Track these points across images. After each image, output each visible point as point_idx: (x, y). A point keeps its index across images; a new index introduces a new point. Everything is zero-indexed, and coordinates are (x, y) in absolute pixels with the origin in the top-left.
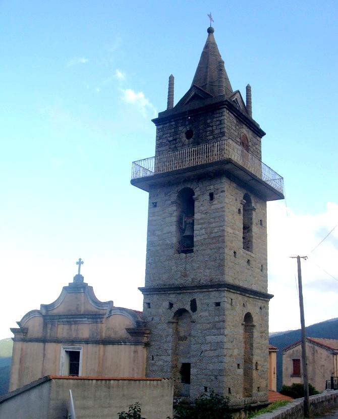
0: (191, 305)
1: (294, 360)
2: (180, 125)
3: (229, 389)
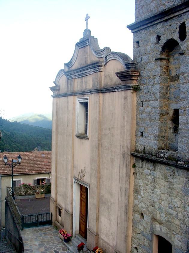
0: (180, 32)
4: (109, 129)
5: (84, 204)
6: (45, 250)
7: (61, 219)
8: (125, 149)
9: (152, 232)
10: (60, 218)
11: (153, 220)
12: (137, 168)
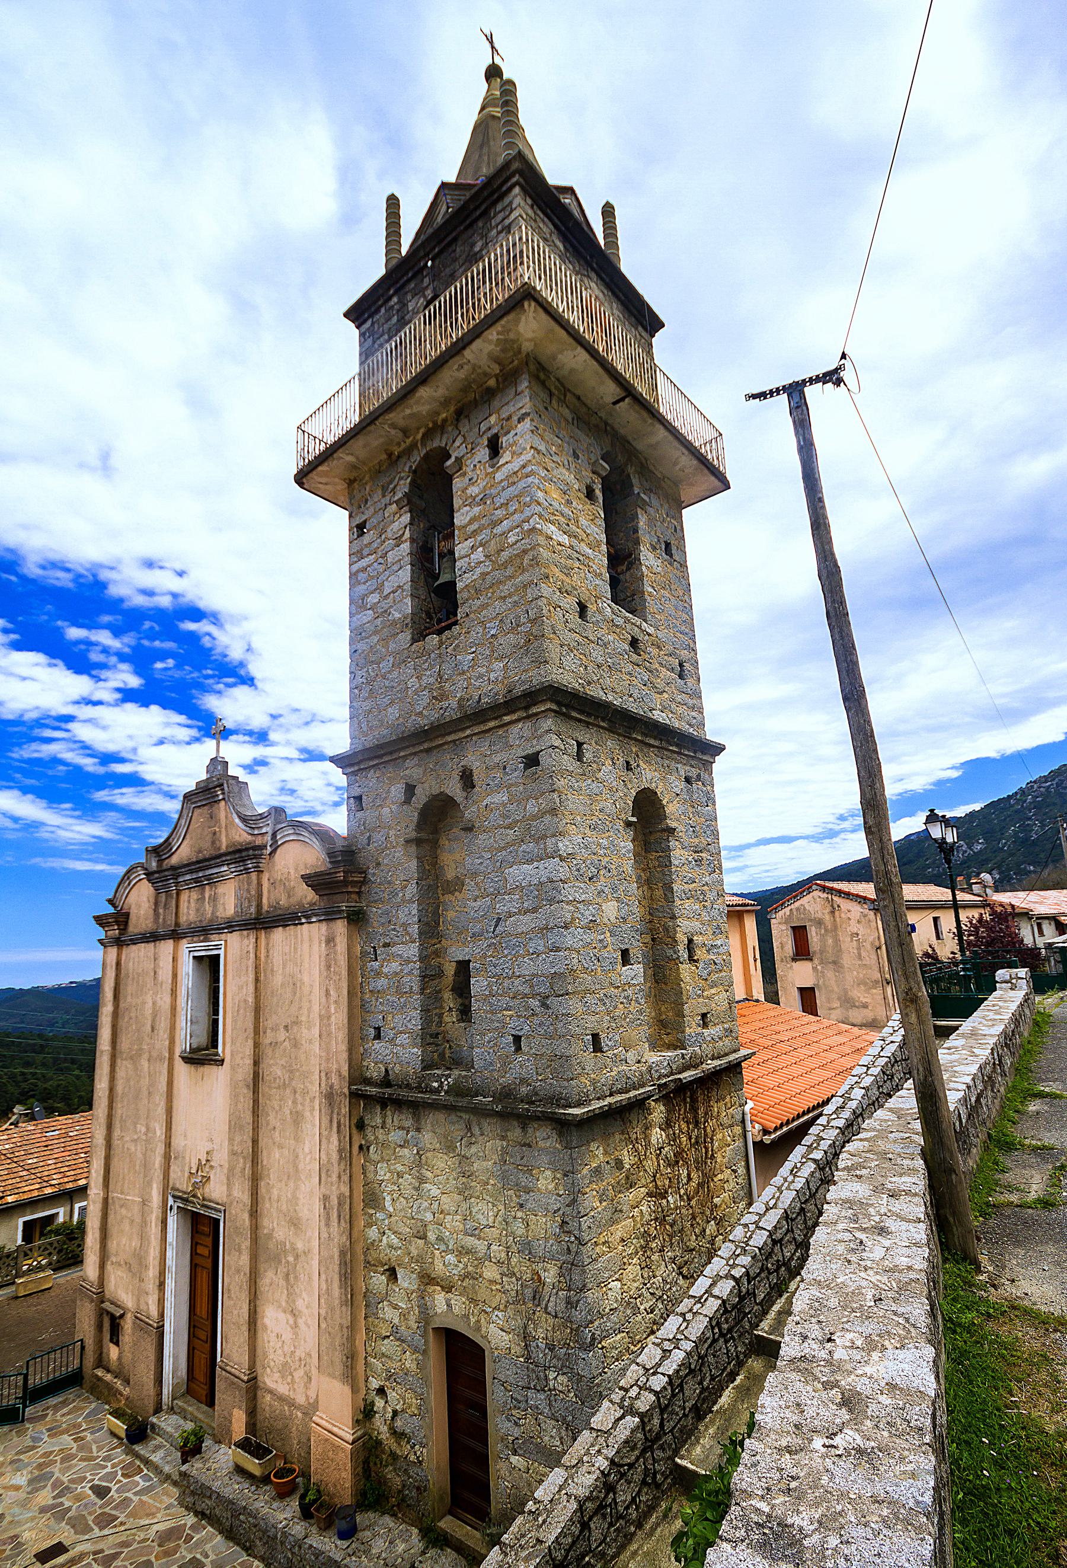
1: (793, 928)
2: (409, 297)
3: (595, 1037)
4: (286, 1027)
5: (204, 1277)
6: (54, 1498)
7: (120, 1353)
8: (334, 1079)
9: (425, 1315)
10: (113, 1352)
11: (426, 1280)
12: (369, 1131)
